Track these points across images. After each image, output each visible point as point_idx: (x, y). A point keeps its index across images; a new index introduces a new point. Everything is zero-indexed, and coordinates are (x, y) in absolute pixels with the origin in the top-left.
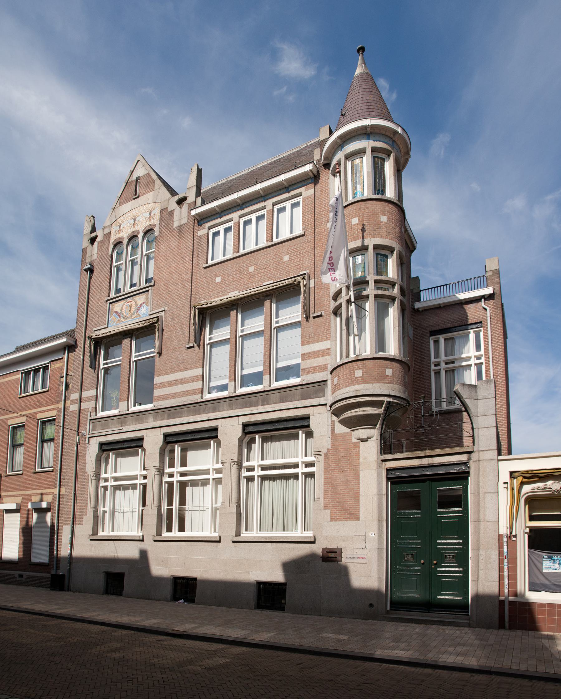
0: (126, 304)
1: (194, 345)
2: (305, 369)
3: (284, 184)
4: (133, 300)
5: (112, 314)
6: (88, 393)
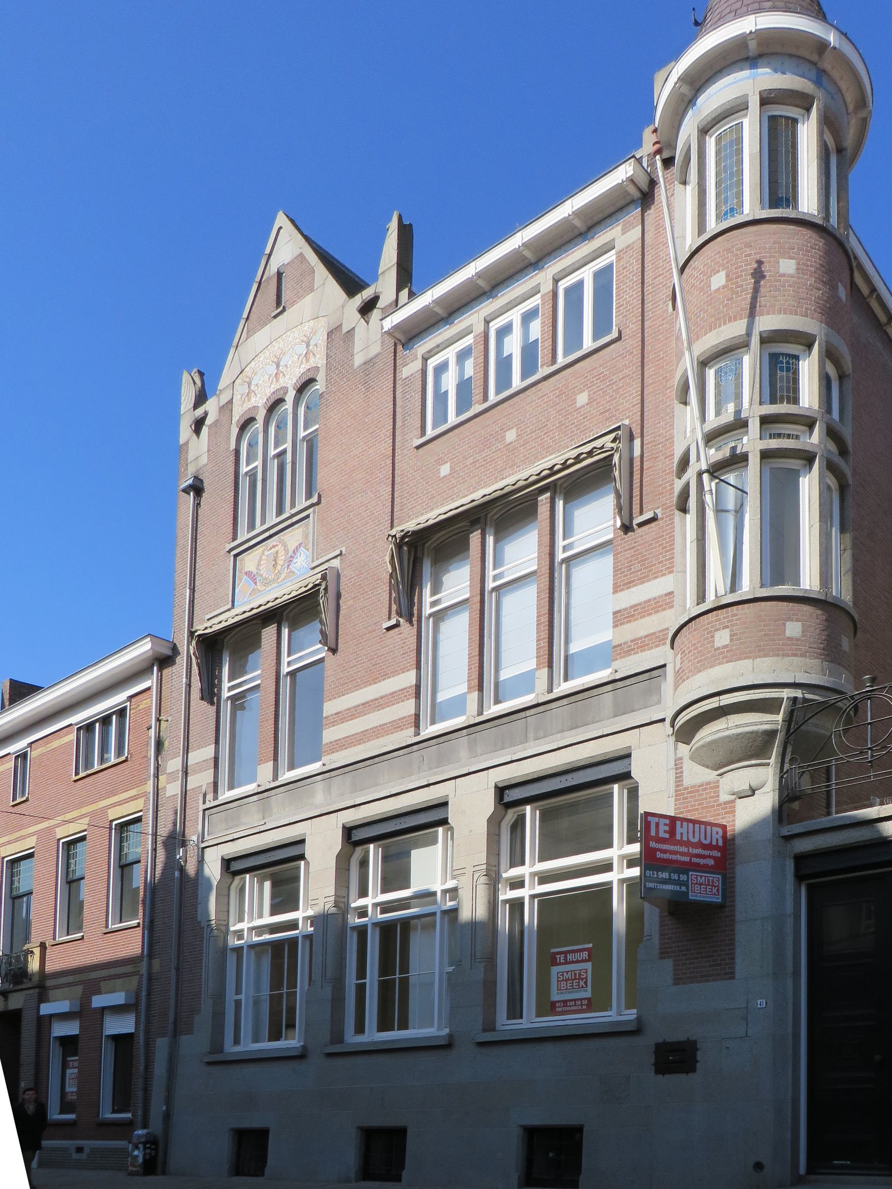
0: (266, 553)
1: (397, 620)
2: (621, 645)
3: (576, 227)
4: (280, 542)
5: (241, 580)
6: (202, 754)
